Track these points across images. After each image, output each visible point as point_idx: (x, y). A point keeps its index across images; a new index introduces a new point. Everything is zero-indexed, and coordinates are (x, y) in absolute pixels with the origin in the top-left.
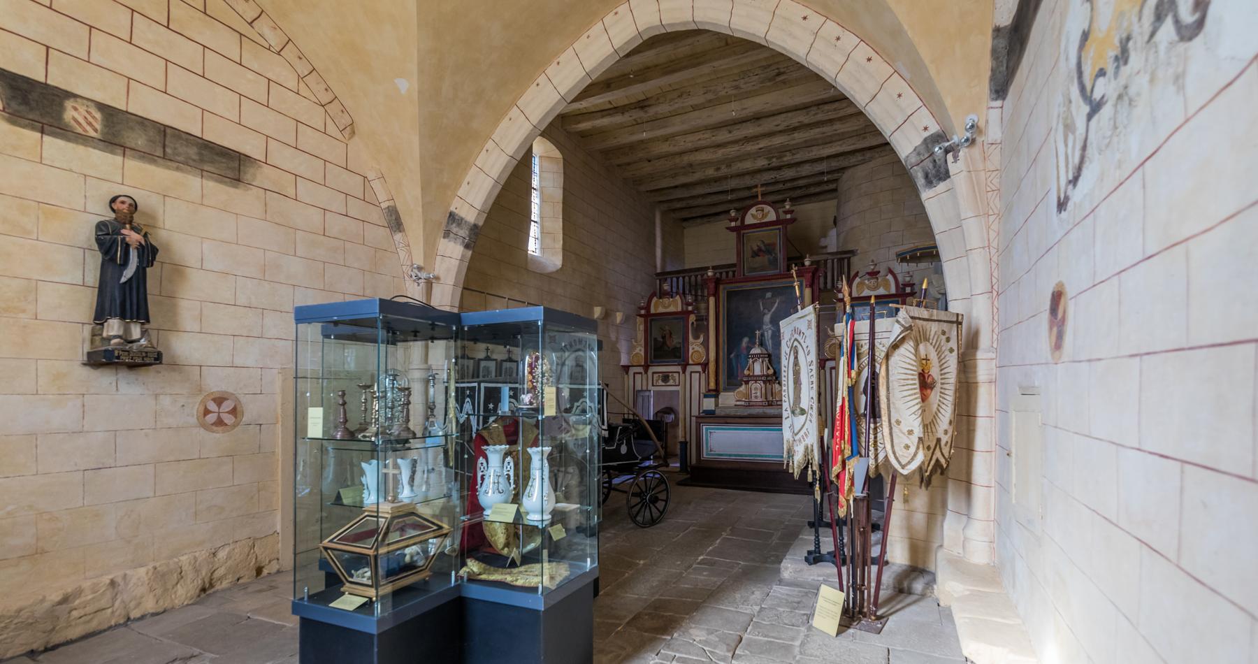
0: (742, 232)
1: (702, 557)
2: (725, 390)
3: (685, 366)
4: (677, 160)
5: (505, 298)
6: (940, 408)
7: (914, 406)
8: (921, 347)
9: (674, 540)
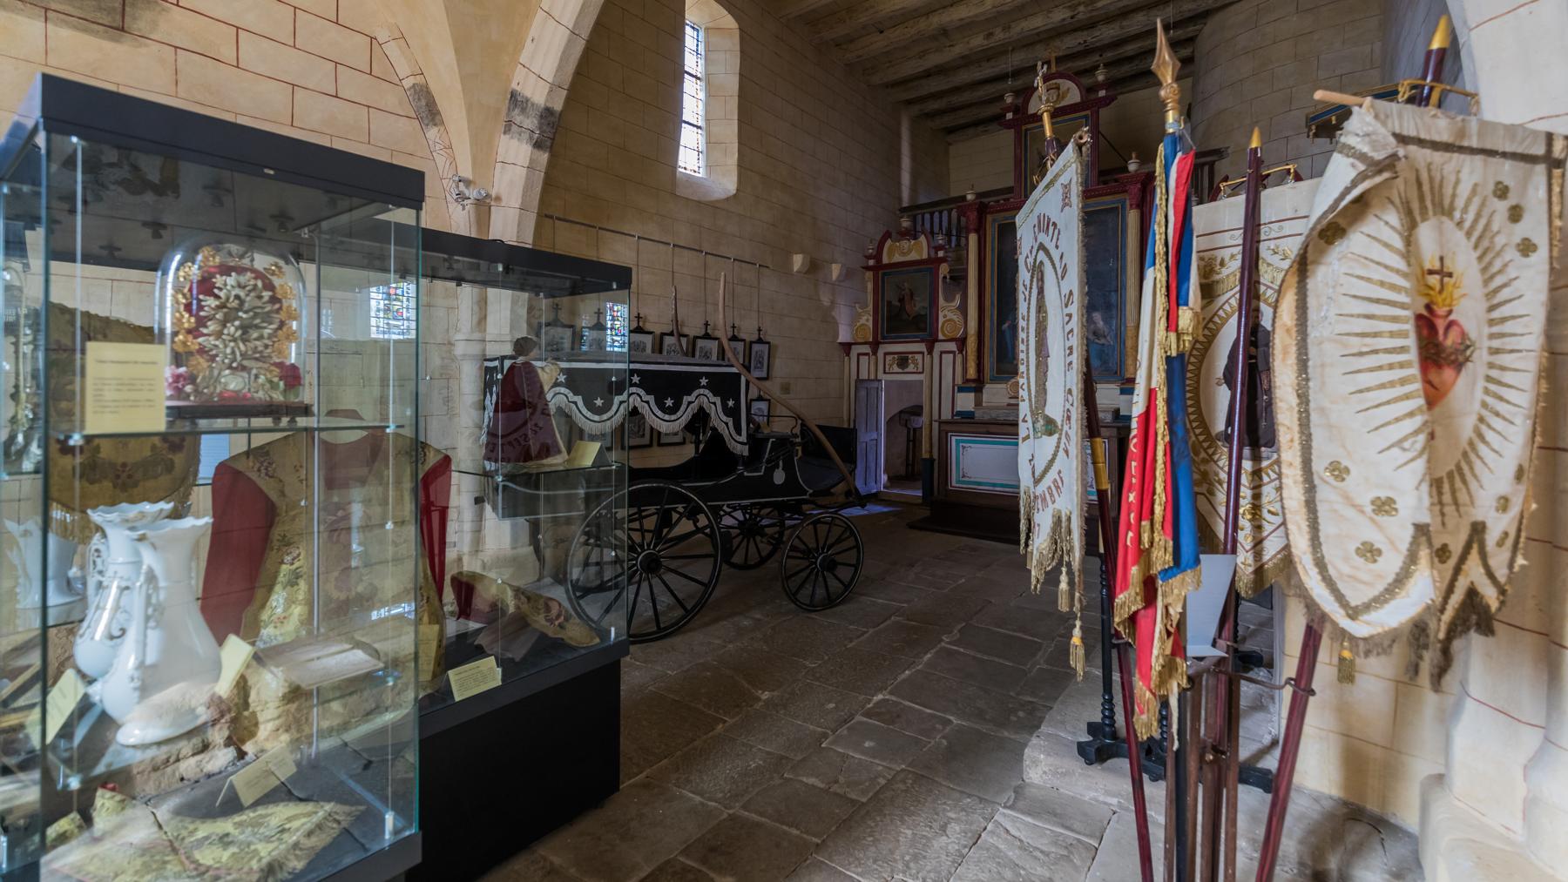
0: (1024, 128)
1: (880, 697)
2: (994, 380)
3: (931, 342)
4: (923, 24)
5: (634, 236)
6: (1483, 428)
7: (1397, 420)
8: (1426, 233)
9: (850, 645)
